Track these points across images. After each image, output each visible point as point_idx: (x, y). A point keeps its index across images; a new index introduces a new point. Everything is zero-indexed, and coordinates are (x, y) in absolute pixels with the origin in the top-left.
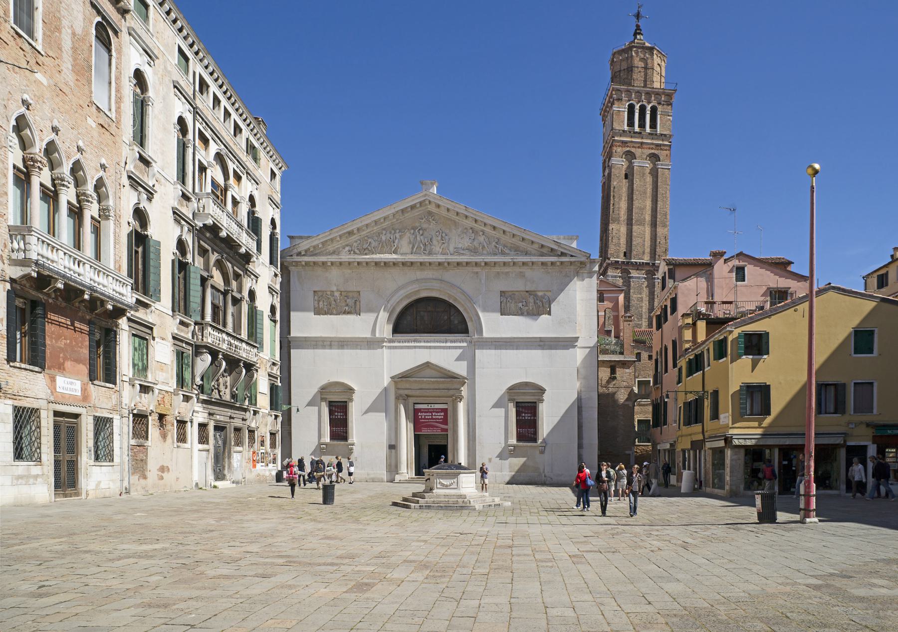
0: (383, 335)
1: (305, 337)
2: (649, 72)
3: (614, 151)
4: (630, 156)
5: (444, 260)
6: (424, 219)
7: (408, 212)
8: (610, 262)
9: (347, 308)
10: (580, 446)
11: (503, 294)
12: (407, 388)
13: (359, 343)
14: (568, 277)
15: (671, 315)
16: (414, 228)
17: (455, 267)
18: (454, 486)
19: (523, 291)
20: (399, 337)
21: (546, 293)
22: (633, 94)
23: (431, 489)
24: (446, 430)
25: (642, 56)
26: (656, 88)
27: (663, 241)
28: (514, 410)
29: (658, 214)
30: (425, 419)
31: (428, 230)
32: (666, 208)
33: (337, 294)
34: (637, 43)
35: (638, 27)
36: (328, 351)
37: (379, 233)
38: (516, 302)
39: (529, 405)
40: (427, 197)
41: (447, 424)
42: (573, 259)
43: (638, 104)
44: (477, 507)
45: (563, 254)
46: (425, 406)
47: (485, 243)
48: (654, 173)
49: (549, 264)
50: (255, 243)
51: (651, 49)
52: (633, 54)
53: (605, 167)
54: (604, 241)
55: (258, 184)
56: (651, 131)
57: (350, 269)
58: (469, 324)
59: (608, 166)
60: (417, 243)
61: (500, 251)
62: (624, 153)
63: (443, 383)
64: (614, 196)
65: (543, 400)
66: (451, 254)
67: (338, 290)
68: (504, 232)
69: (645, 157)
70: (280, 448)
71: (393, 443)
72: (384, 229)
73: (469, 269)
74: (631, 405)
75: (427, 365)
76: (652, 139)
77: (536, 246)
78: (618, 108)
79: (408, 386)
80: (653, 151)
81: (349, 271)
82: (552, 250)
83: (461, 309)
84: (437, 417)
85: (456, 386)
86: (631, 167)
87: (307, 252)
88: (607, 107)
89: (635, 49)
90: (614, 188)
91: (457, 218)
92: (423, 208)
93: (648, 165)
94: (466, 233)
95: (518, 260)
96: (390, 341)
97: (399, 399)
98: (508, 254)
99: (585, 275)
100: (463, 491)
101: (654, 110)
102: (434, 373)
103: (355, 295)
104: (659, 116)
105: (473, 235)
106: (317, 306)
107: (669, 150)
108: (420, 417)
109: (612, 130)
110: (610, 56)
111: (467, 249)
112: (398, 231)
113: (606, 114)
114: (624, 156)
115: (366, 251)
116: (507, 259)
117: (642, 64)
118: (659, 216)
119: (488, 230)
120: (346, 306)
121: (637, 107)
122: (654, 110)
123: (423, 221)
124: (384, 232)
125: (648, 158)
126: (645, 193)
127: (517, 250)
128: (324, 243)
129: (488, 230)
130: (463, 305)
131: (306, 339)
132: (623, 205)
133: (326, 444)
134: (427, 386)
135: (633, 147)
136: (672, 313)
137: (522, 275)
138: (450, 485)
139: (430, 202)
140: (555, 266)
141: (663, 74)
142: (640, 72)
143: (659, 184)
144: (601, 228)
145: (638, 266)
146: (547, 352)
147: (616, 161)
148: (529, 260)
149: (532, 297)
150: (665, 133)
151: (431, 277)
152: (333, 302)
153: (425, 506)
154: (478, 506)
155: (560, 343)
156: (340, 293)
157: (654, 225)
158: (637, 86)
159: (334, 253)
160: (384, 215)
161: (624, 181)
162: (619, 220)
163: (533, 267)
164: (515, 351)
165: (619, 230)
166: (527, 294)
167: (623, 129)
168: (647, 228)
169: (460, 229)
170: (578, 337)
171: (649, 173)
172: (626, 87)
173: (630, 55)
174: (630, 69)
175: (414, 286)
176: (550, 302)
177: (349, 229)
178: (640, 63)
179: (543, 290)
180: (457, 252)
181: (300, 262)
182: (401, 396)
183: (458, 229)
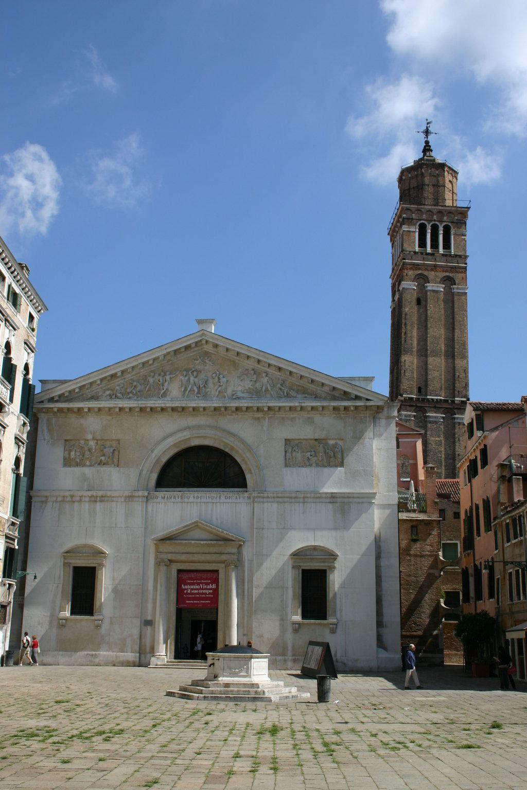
4: (422, 279)
7: (181, 353)
8: (403, 399)
9: (103, 458)
11: (288, 443)
15: (481, 468)
16: (187, 370)
17: (233, 412)
19: (311, 439)
23: (216, 677)
26: (448, 206)
29: (456, 344)
35: (427, 142)
38: (303, 452)
44: (273, 699)
45: (357, 398)
49: (342, 409)
50: (9, 392)
53: (395, 291)
54: (395, 374)
55: (15, 329)
58: (248, 477)
59: (399, 290)
60: (190, 386)
61: (285, 394)
63: (214, 545)
67: (93, 439)
68: (291, 373)
69: (439, 280)
70: (10, 623)
71: (149, 618)
72: (151, 372)
79: (171, 549)
80: (447, 274)
82: (345, 392)
83: (239, 460)
92: (198, 348)
100: (255, 679)
102: (204, 535)
103: (114, 444)
105: (255, 376)
106: (67, 456)
112: (168, 373)
113: (395, 234)
116: (295, 404)
118: (457, 347)
119: (271, 371)
120: (102, 456)
123: (198, 362)
124: (152, 374)
127: (304, 391)
129: (271, 371)
133: (66, 619)
134: (195, 550)
136: (483, 466)
137: (310, 421)
139: (207, 342)
140: (348, 411)
143: (455, 310)
145: (436, 405)
150: (460, 254)
153: (211, 697)
154: (274, 698)
160: (154, 356)
163: (324, 412)
167: (414, 250)
169: (240, 370)
170: (376, 493)
173: (419, 172)
181: (52, 408)
182: (163, 561)
183: (238, 370)
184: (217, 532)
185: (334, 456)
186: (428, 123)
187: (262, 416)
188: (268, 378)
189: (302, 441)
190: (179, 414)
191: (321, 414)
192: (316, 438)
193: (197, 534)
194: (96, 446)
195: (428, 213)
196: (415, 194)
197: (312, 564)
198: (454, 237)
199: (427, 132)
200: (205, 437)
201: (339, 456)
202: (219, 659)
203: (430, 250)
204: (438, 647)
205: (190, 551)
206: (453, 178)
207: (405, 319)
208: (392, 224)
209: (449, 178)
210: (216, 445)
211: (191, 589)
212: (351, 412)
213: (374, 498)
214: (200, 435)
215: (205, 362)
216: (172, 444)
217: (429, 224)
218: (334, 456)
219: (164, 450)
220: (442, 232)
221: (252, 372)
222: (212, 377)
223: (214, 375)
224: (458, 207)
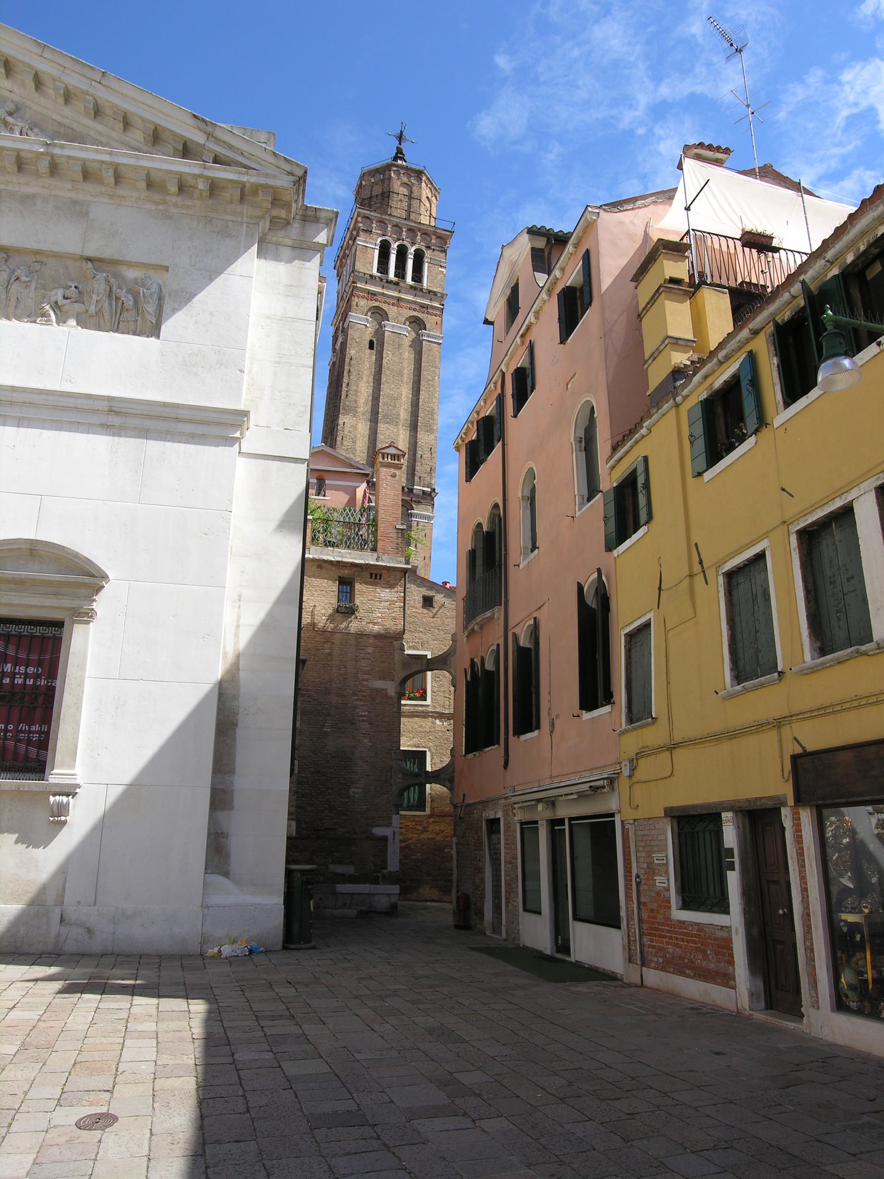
2: (415, 203)
14: (230, 236)
22: (390, 226)
25: (405, 180)
32: (433, 403)
35: (399, 151)
38: (44, 287)
48: (417, 346)
62: (370, 309)
69: (404, 319)
78: (365, 242)
80: (415, 314)
88: (347, 248)
89: (395, 169)
95: (66, 152)
101: (419, 258)
104: (426, 266)
109: (353, 272)
114: (369, 314)
118: (421, 414)
121: (395, 246)
125: (408, 323)
126: (401, 374)
135: (385, 302)
142: (401, 201)
146: (128, 445)
148: (106, 158)
149: (101, 276)
150: (435, 290)
161: (368, 351)
163: (120, 192)
173: (387, 176)
174: (386, 195)
176: (160, 299)
178: (401, 189)
189: (45, 259)
191: (111, 197)
192: (90, 252)
195: (395, 228)
197: (15, 600)
198: (428, 267)
199: (400, 138)
201: (151, 308)
203: (393, 277)
204: (385, 868)
206: (432, 197)
213: (239, 426)
220: (412, 257)
224: (437, 228)
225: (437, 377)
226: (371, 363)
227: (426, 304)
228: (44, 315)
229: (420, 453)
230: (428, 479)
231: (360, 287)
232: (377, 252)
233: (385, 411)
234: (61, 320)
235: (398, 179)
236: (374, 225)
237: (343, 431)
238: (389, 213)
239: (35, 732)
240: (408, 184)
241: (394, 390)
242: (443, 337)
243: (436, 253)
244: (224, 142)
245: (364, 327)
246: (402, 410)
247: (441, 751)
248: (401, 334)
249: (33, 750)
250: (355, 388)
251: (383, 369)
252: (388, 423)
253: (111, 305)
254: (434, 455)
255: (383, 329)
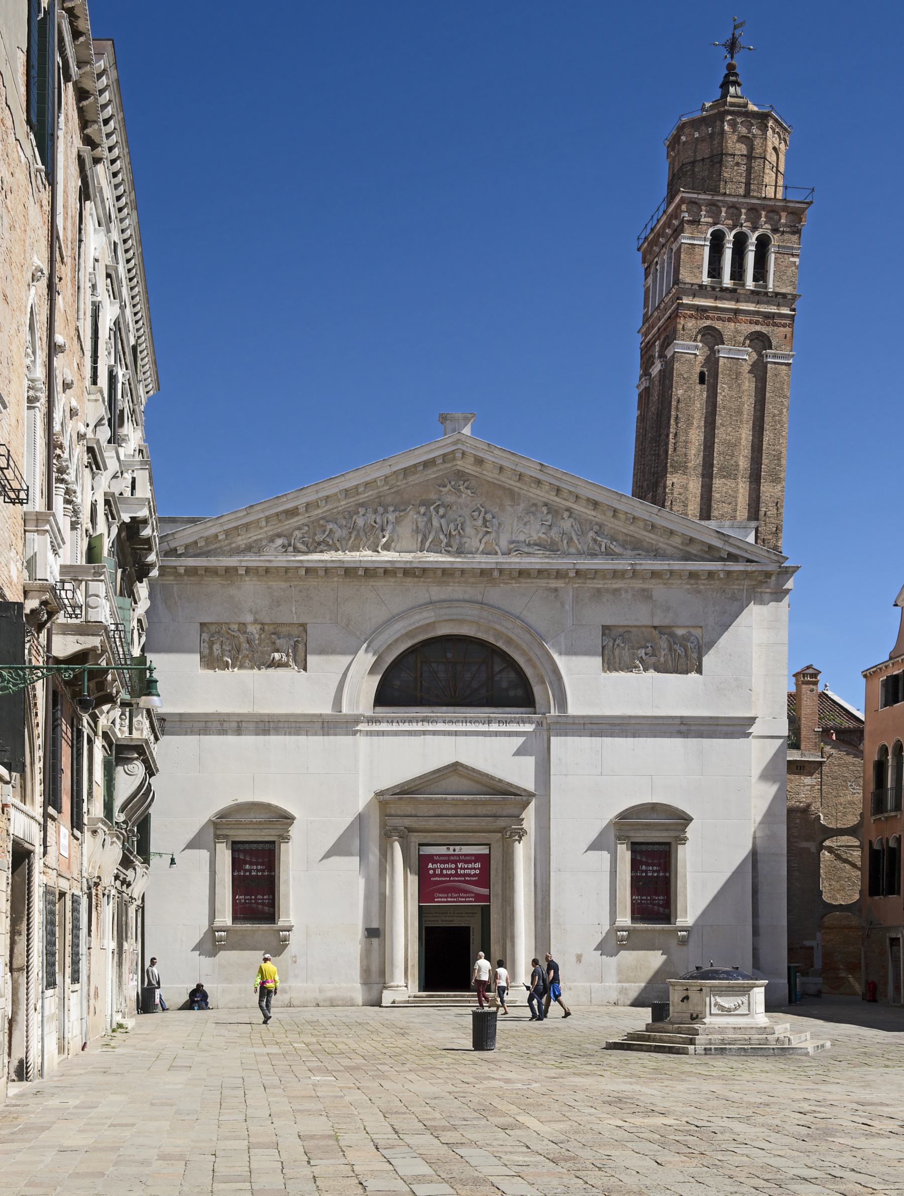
0: (358, 708)
1: (180, 715)
2: (756, 164)
3: (680, 327)
4: (712, 337)
5: (493, 566)
6: (449, 487)
10: (756, 932)
12: (409, 813)
13: (302, 725)
14: (737, 600)
18: (743, 1010)
20: (383, 711)
21: (693, 631)
22: (724, 210)
24: (487, 898)
25: (743, 130)
27: (772, 511)
28: (628, 855)
30: (442, 875)
31: (455, 508)
33: (253, 629)
34: (732, 105)
35: (731, 67)
36: (231, 739)
37: (349, 512)
39: (656, 848)
40: (459, 446)
41: (487, 885)
42: (751, 567)
43: (731, 229)
46: (442, 850)
47: (573, 533)
48: (759, 371)
51: (763, 118)
52: (726, 127)
56: (756, 286)
57: (286, 581)
58: (537, 690)
61: (603, 549)
64: (677, 418)
65: (685, 839)
66: (503, 554)
67: (256, 622)
69: (742, 339)
72: (362, 505)
73: (542, 583)
74: (813, 850)
75: (455, 768)
76: (758, 303)
77: (677, 541)
79: (409, 810)
80: (758, 328)
81: (284, 585)
82: (711, 547)
84: (467, 871)
85: (512, 811)
86: (712, 361)
87: (192, 550)
89: (729, 117)
90: (678, 401)
91: (518, 484)
93: (748, 355)
94: (534, 514)
95: (643, 567)
96: (371, 720)
97: (390, 837)
98: (619, 556)
99: (767, 597)
101: (763, 244)
102: (465, 784)
103: (295, 631)
104: (773, 256)
105: (549, 517)
107: (791, 326)
108: (431, 872)
110: (670, 130)
111: (537, 545)
114: (699, 337)
115: (322, 547)
116: (622, 564)
117: (742, 149)
118: (765, 461)
121: (730, 237)
122: (763, 244)
124: (362, 511)
126: (739, 412)
127: (637, 547)
128: (227, 533)
129: (579, 508)
130: (524, 653)
131: (182, 718)
132: (696, 436)
134: (451, 811)
135: (719, 319)
137: (646, 595)
138: (736, 1009)
139: (463, 453)
140: (714, 579)
141: (782, 168)
143: (768, 395)
144: (633, 481)
147: (683, 347)
148: (666, 567)
150: (783, 291)
151: (461, 597)
152: (245, 645)
155: (719, 728)
156: (259, 627)
157: (755, 478)
158: (730, 195)
159: (249, 549)
160: (368, 479)
161: (698, 387)
162: (686, 467)
163: (670, 581)
164: (630, 740)
165: (685, 487)
166: (655, 633)
167: (698, 281)
168: (741, 485)
171: (750, 372)
172: (710, 197)
173: (717, 129)
174: (717, 159)
175: (425, 614)
177: (289, 506)
178: (739, 145)
179: (688, 624)
180: (515, 548)
182: (395, 829)
184: (491, 782)
185: (686, 655)
186: (735, 28)
187: (563, 585)
188: (571, 520)
189: (630, 629)
190: (416, 580)
192: (656, 624)
193: (454, 782)
194: (260, 635)
195: (731, 211)
196: (706, 173)
198: (776, 259)
200: (461, 622)
202: (701, 990)
204: (812, 967)
205: (443, 813)
207: (677, 409)
208: (652, 230)
209: (773, 143)
210: (481, 635)
211: (442, 870)
212: (717, 582)
214: (454, 617)
215: (459, 490)
216: (404, 631)
217: (731, 232)
218: (686, 655)
219: (389, 642)
221: (545, 510)
222: (472, 516)
223: (476, 514)
224: (789, 201)
225: (785, 410)
226: (702, 402)
227: (772, 313)
228: (636, 667)
229: (764, 509)
230: (773, 541)
231: (687, 304)
232: (707, 250)
233: (721, 463)
234: (646, 670)
235: (734, 132)
236: (703, 213)
237: (672, 494)
238: (722, 191)
239: (266, 899)
240: (748, 137)
241: (731, 434)
242: (793, 356)
243: (786, 236)
244: (735, 545)
245: (693, 356)
246: (741, 458)
247: (830, 876)
248: (739, 359)
249: (661, 909)
250: (684, 438)
251: (718, 409)
252: (724, 477)
253: (671, 655)
254: (781, 510)
255: (717, 356)
